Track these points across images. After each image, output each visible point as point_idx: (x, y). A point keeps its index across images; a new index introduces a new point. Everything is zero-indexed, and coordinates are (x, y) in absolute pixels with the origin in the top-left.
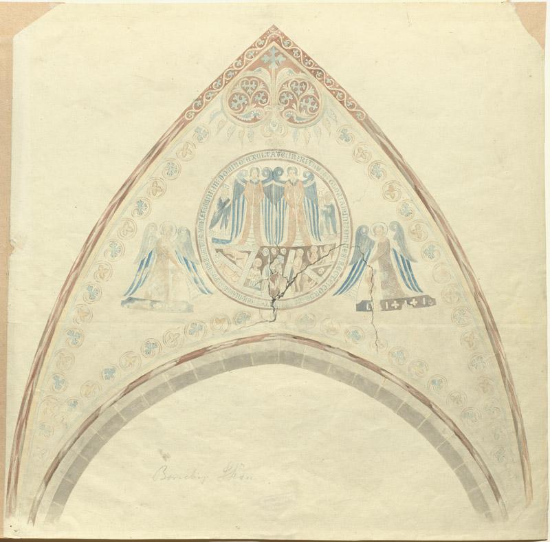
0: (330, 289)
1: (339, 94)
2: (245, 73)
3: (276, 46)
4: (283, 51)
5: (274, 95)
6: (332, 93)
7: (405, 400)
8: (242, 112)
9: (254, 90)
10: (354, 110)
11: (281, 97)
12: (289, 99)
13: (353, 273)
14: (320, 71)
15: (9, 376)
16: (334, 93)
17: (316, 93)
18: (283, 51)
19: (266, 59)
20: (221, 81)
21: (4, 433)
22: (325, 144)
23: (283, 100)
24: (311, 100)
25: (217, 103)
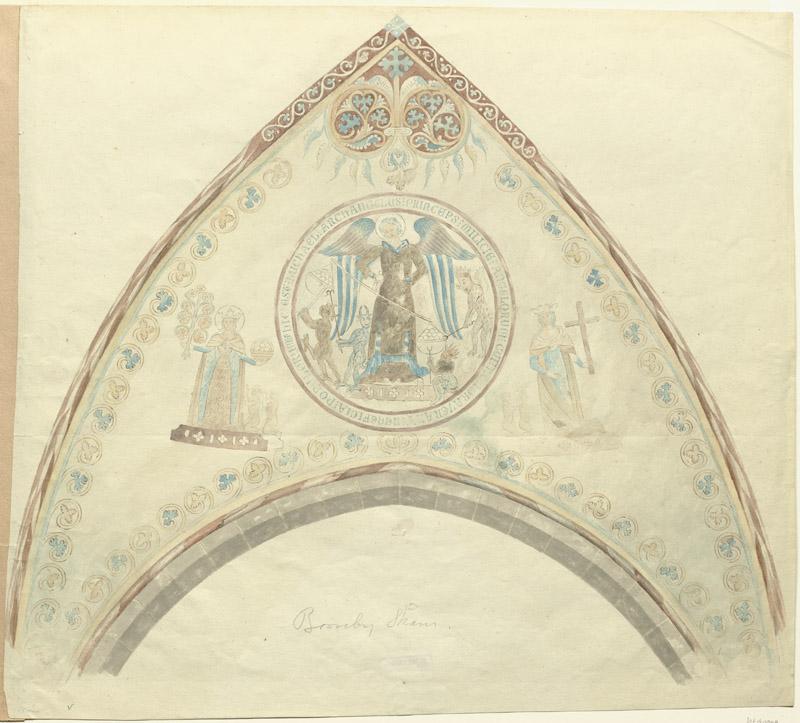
0: (324, 218)
1: (460, 83)
2: (356, 83)
3: (404, 51)
4: (408, 51)
5: (397, 113)
6: (507, 140)
7: (594, 560)
8: (352, 138)
9: (370, 107)
10: (512, 135)
11: (408, 116)
12: (417, 113)
13: (440, 287)
14: (490, 108)
15: (20, 406)
16: (510, 139)
17: (456, 110)
18: (408, 51)
19: (386, 64)
20: (323, 88)
21: (8, 458)
22: (467, 181)
23: (411, 120)
24: (449, 120)
25: (320, 119)
